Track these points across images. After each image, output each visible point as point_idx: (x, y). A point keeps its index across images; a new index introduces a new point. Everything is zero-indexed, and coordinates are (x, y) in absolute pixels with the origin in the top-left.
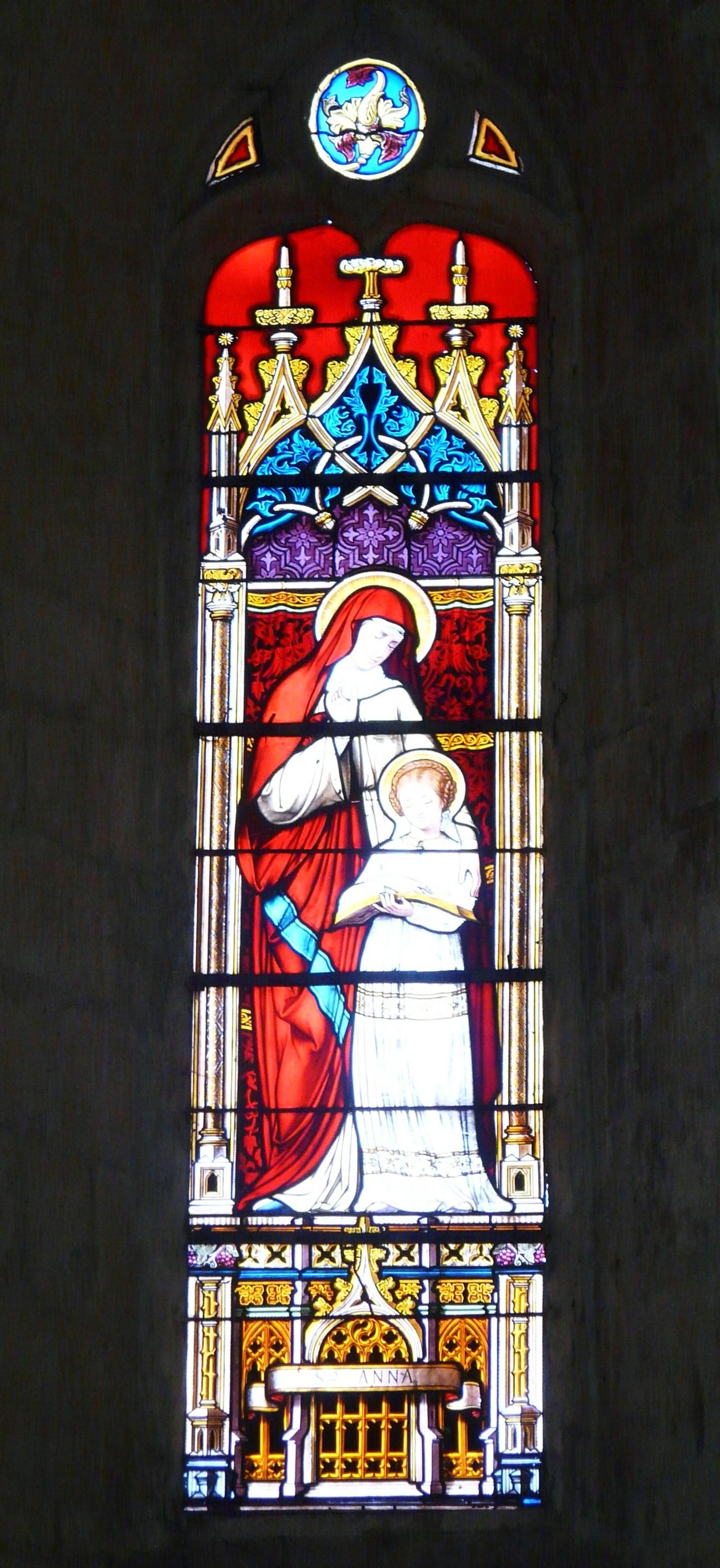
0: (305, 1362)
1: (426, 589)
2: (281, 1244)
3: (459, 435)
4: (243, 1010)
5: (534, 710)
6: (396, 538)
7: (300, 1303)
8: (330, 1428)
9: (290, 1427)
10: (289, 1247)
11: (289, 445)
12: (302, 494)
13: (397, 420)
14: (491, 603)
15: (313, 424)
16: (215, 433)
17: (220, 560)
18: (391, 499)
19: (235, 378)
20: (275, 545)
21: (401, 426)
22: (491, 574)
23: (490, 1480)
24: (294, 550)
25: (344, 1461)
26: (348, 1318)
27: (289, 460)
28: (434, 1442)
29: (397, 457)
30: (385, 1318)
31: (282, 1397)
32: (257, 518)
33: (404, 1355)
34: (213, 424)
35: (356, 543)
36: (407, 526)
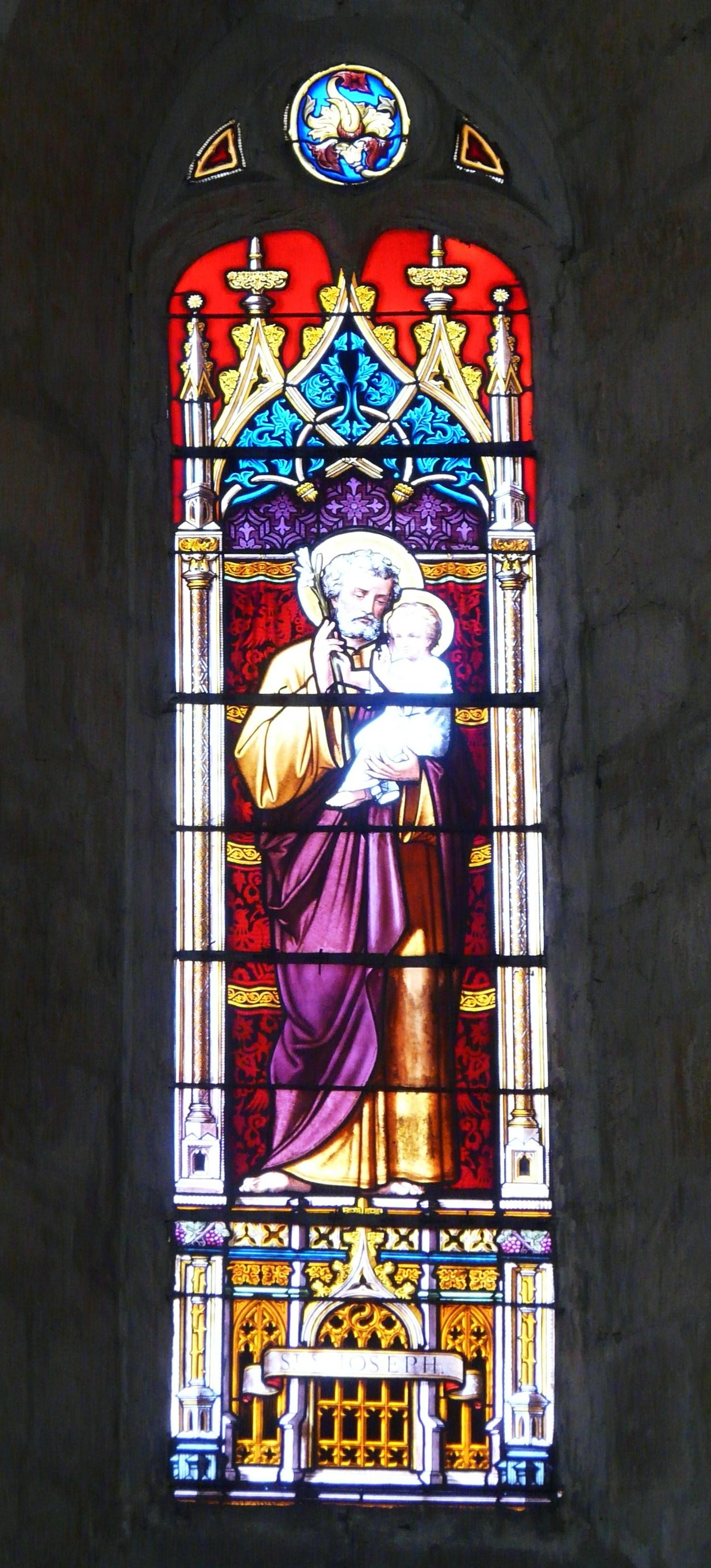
0: (303, 1345)
1: (419, 561)
2: (280, 1223)
3: (443, 407)
4: (229, 986)
5: (531, 685)
6: (381, 511)
7: (298, 1285)
8: (328, 1414)
9: (287, 1410)
10: (416, 1232)
11: (269, 417)
12: (283, 466)
13: (377, 389)
14: (485, 578)
15: (293, 395)
16: (496, 395)
17: (194, 532)
18: (373, 471)
19: (207, 345)
20: (254, 515)
21: (381, 395)
22: (484, 549)
23: (494, 1472)
24: (273, 521)
25: (343, 1449)
26: (348, 1301)
27: (271, 433)
28: (434, 1431)
29: (380, 428)
30: (379, 1302)
31: (279, 1380)
32: (236, 488)
33: (403, 1340)
34: (493, 388)
35: (340, 515)
36: (391, 500)
